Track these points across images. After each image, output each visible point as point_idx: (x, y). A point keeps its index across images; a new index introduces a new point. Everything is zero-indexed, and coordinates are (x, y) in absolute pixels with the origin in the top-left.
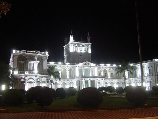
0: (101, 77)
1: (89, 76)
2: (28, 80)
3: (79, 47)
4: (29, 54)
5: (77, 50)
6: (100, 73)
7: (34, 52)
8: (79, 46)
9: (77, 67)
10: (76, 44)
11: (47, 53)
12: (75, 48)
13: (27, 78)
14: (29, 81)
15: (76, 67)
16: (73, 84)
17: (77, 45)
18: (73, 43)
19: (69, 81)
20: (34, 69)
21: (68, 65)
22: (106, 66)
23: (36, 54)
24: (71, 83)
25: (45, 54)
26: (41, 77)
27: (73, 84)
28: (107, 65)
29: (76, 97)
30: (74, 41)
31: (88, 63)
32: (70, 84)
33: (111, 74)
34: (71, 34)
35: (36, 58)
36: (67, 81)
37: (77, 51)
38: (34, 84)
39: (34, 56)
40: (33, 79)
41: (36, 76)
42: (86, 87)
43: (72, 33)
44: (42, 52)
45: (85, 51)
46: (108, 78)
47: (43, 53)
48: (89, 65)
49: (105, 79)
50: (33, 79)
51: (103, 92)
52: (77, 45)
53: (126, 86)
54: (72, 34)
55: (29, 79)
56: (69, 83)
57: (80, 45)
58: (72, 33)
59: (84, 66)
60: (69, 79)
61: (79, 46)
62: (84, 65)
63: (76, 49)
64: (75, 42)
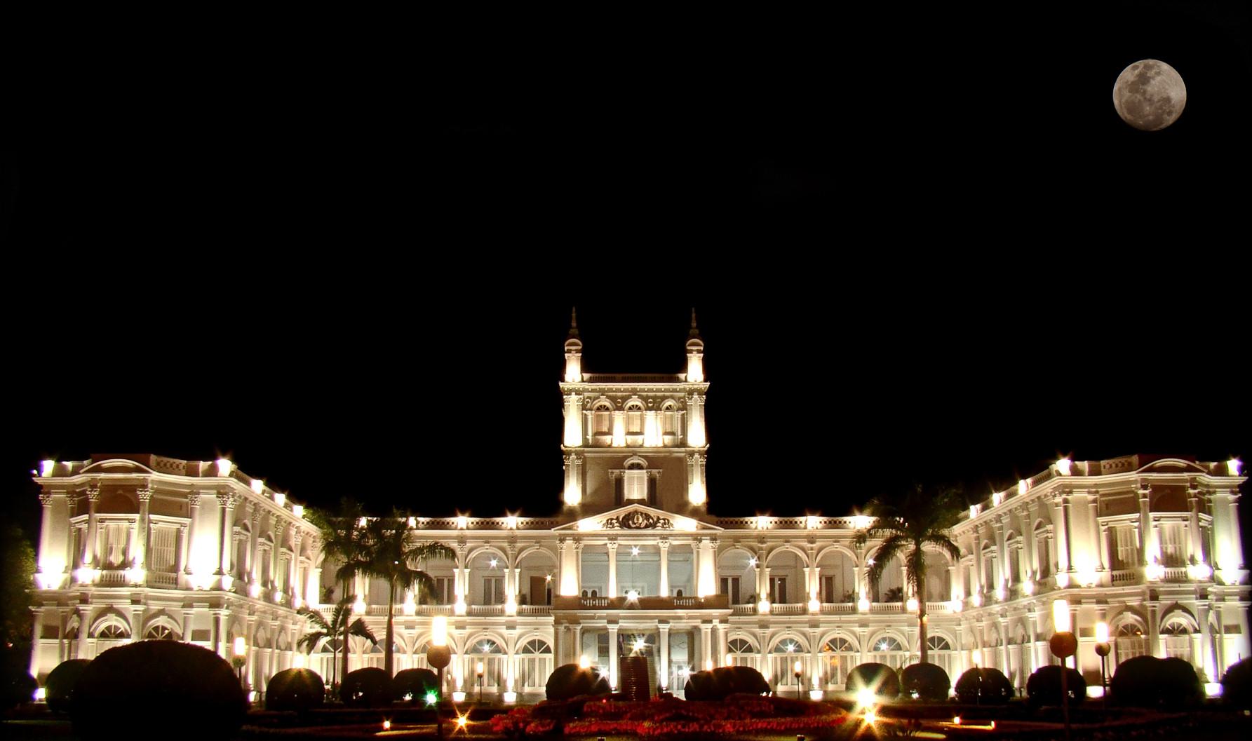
0: (690, 602)
1: (696, 598)
2: (95, 620)
3: (619, 418)
4: (102, 475)
5: (609, 433)
6: (488, 581)
7: (1181, 463)
8: (621, 409)
9: (569, 542)
10: (603, 392)
11: (1233, 465)
12: (599, 420)
13: (89, 610)
14: (102, 625)
15: (562, 540)
16: (947, 647)
17: (607, 403)
18: (578, 393)
19: (468, 630)
20: (131, 558)
21: (510, 533)
22: (792, 525)
23: (141, 475)
24: (532, 643)
25: (1221, 471)
26: (183, 606)
27: (947, 647)
28: (802, 519)
29: (507, 722)
30: (586, 376)
31: (647, 517)
32: (526, 650)
33: (490, 581)
34: (691, 331)
35: (145, 497)
36: (858, 630)
37: (607, 439)
38: (1194, 635)
39: (132, 488)
40: (120, 614)
41: (1203, 596)
42: (561, 665)
43: (694, 325)
44: (195, 463)
45: (668, 439)
46: (854, 610)
47: (203, 465)
48: (654, 526)
49: (731, 619)
50: (120, 614)
51: (914, 701)
52: (607, 403)
53: (722, 665)
54: (697, 331)
55: (1169, 610)
56: (826, 639)
57: (625, 399)
58: (694, 325)
59: (613, 538)
60: (822, 618)
61: (619, 403)
62: (617, 530)
63: (605, 429)
64: (591, 380)
